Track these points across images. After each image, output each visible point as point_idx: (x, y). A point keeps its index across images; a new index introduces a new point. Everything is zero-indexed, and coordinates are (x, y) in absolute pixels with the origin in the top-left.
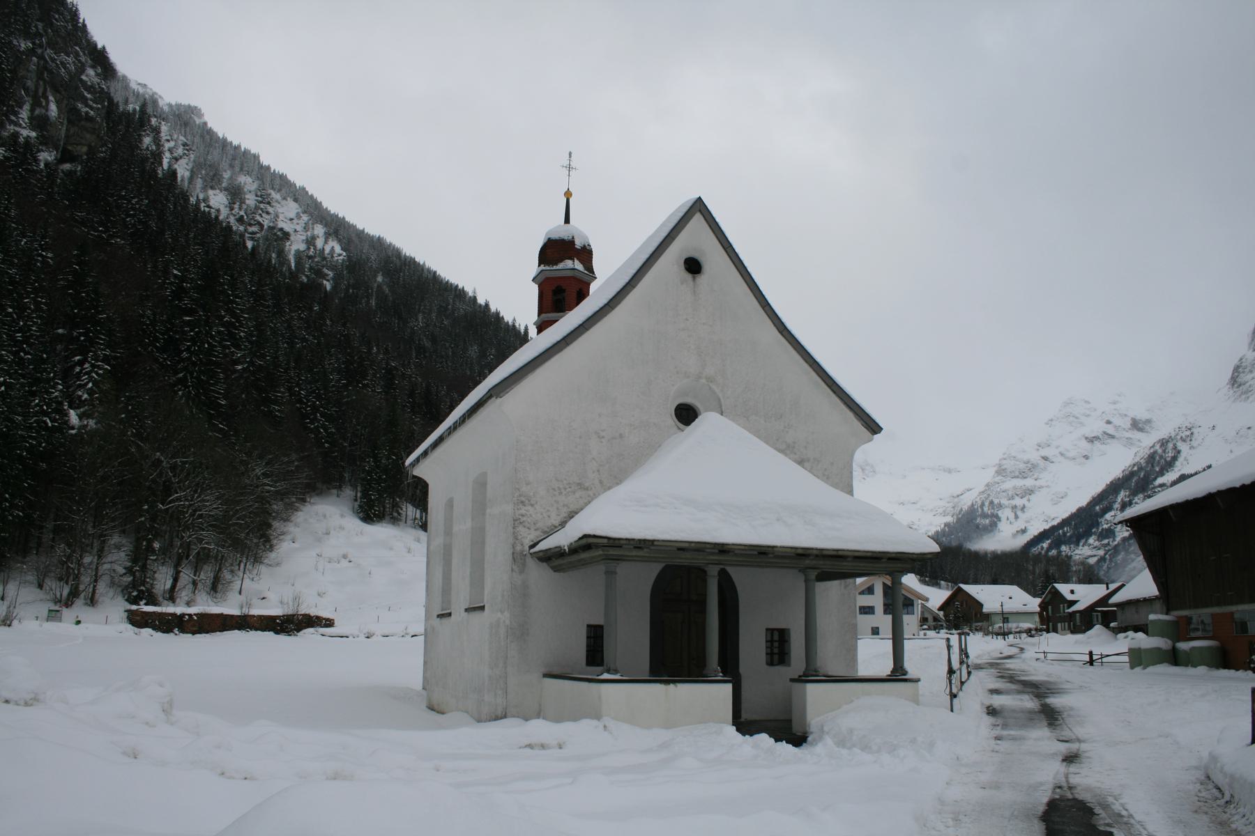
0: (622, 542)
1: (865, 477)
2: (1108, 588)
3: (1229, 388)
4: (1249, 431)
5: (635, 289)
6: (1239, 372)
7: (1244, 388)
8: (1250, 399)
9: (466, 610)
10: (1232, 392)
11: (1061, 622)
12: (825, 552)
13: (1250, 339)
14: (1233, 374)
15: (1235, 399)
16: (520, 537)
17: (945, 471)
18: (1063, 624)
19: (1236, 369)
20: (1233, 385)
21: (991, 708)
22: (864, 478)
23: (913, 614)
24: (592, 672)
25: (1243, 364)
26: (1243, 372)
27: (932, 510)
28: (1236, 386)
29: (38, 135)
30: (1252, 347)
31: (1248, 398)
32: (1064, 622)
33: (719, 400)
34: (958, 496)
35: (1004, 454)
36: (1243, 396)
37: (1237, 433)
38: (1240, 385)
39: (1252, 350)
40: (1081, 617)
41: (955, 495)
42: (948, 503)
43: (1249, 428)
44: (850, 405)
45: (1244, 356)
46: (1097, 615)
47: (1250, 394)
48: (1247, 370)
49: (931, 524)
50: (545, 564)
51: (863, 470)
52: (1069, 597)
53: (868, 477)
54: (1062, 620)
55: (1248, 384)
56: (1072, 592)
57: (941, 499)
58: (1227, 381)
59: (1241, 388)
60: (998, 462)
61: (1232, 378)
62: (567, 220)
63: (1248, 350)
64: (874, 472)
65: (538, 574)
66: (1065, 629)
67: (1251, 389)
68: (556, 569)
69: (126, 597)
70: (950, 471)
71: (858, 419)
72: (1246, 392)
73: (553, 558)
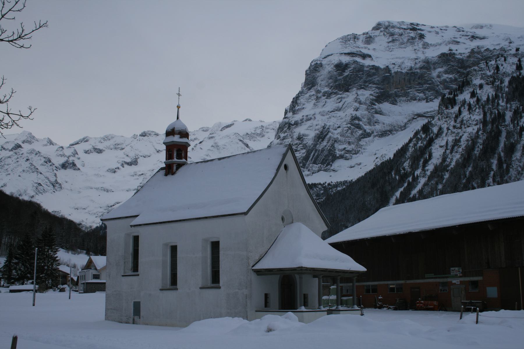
1: (55, 191)
9: (201, 288)
13: (276, 133)
17: (104, 190)
22: (54, 192)
24: (266, 309)
27: (95, 214)
33: (292, 215)
34: (111, 206)
35: (141, 183)
39: (276, 139)
41: (110, 205)
42: (105, 210)
45: (272, 141)
50: (255, 273)
51: (54, 186)
53: (56, 191)
57: (101, 208)
60: (136, 188)
62: (178, 118)
63: (275, 139)
64: (61, 188)
65: (254, 276)
68: (258, 275)
70: (108, 191)
73: (259, 272)
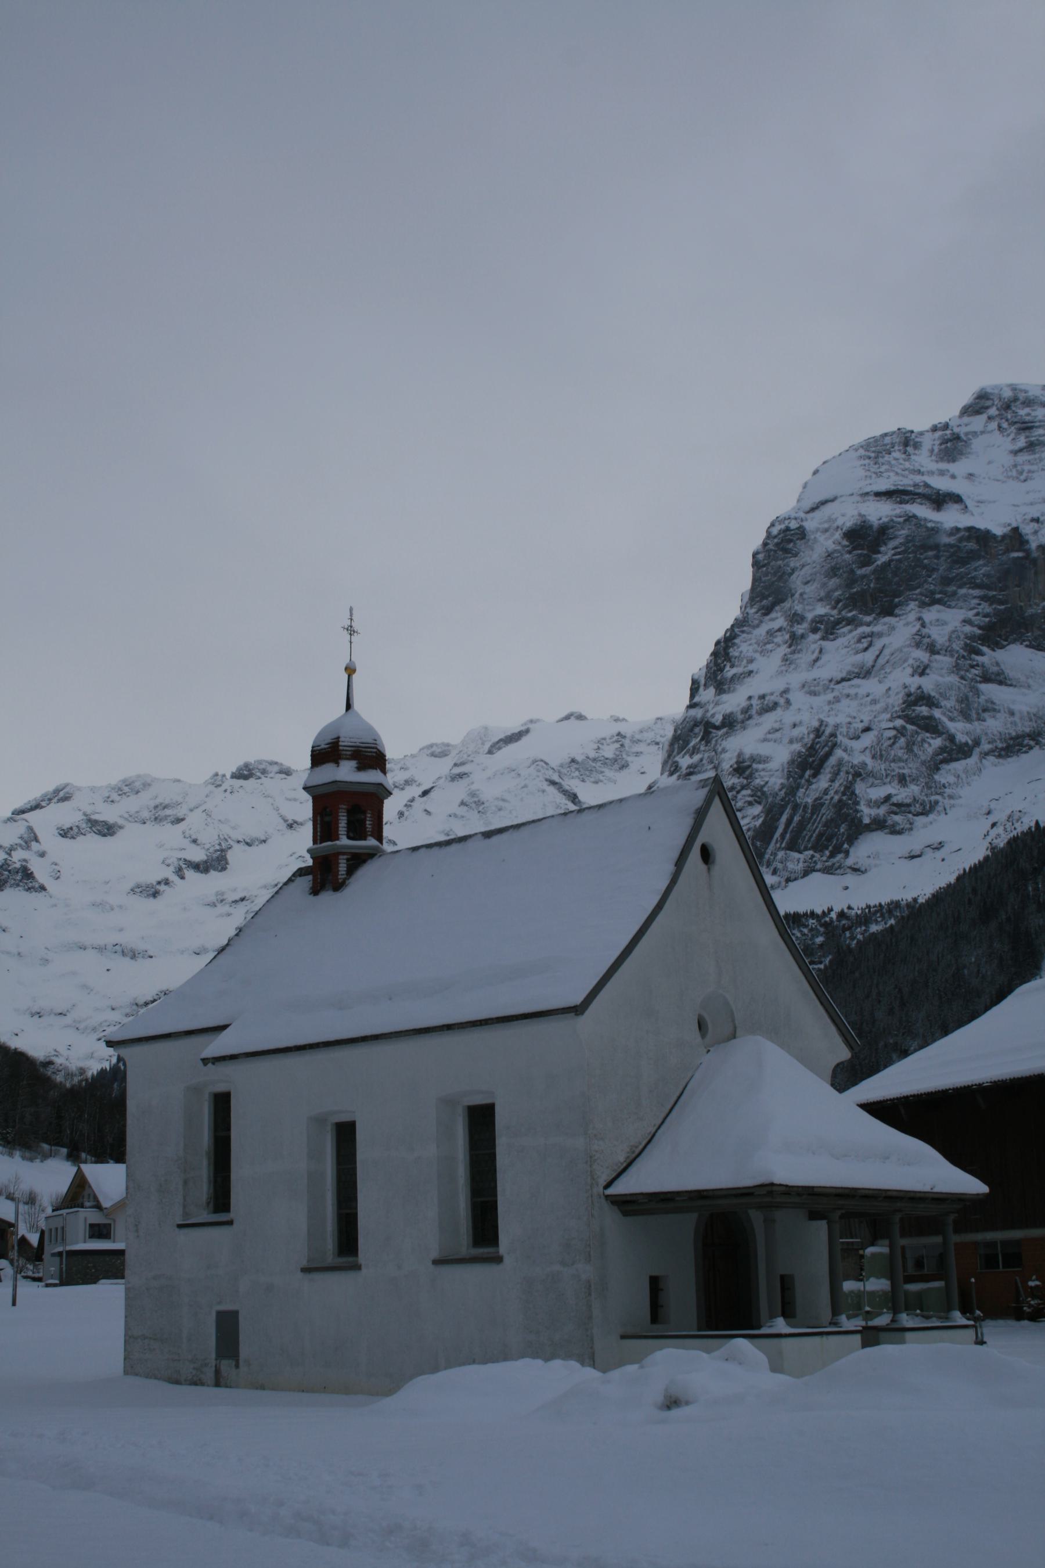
0: (775, 1188)
5: (677, 885)
9: (436, 1262)
12: (889, 1193)
16: (595, 1177)
17: (124, 954)
23: (110, 1238)
27: (94, 1029)
29: (861, 915)
30: (668, 769)
34: (146, 1004)
39: (667, 773)
41: (141, 1001)
42: (127, 1015)
49: (91, 1056)
62: (349, 706)
63: (662, 774)
65: (611, 1218)
68: (625, 1214)
70: (134, 956)
71: (839, 1035)
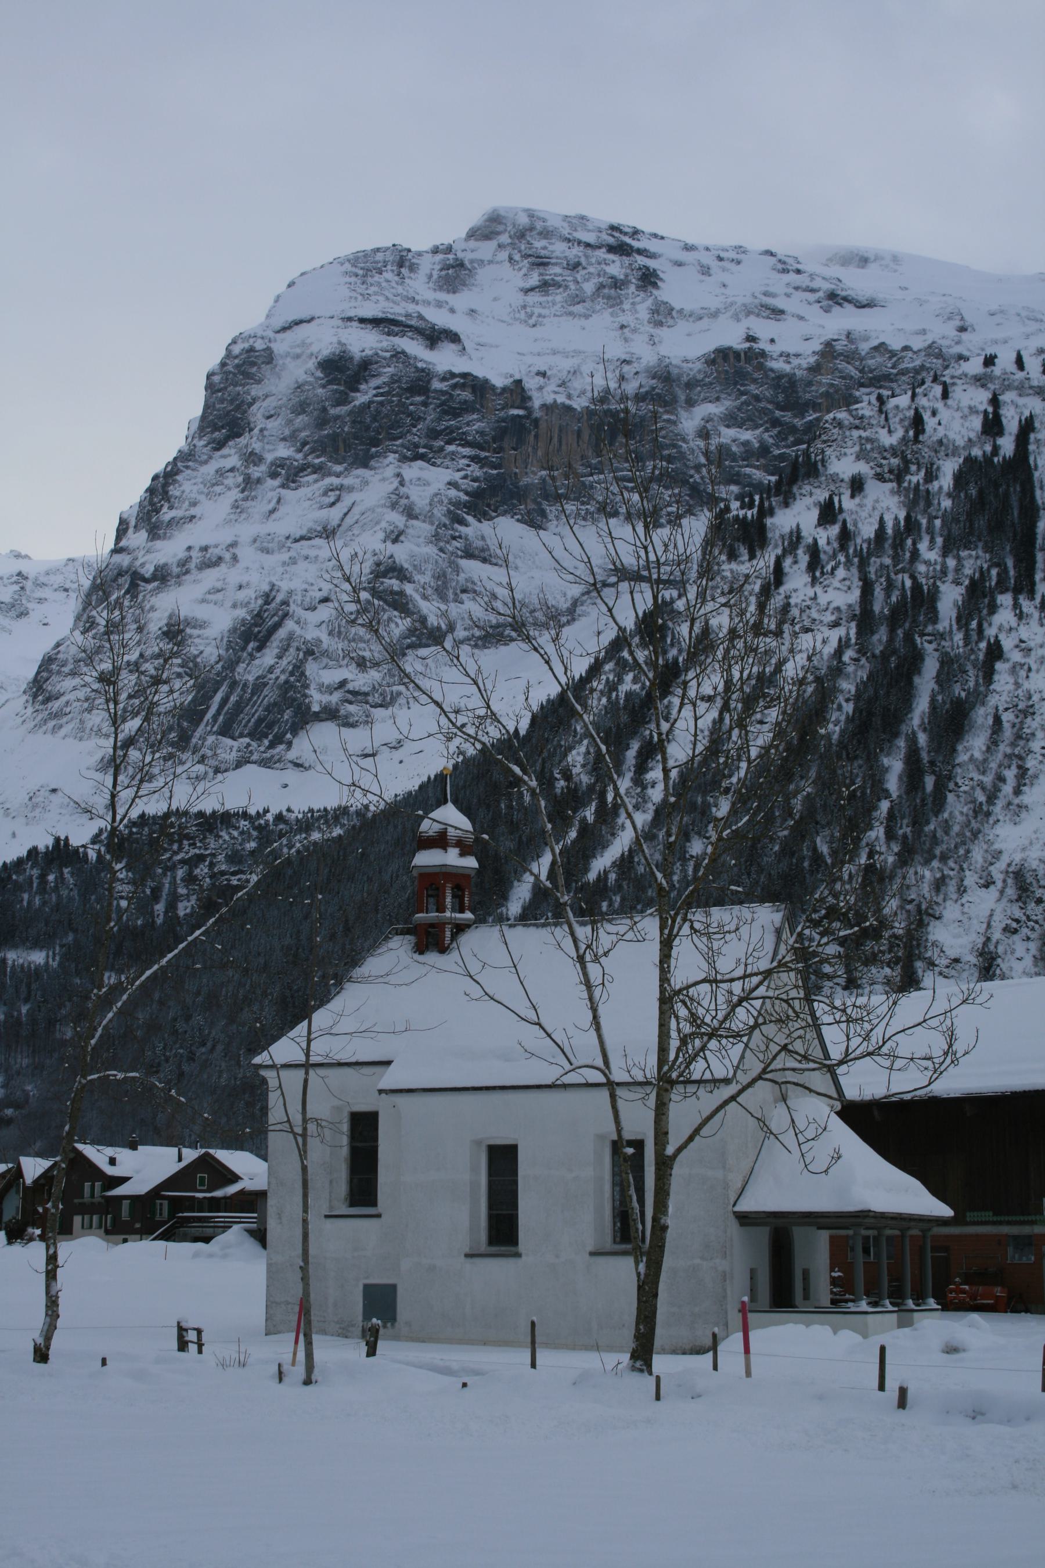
2: (180, 1159)
3: (27, 701)
4: (53, 797)
6: (50, 672)
7: (55, 705)
8: (63, 732)
10: (30, 710)
11: (82, 1214)
14: (38, 673)
15: (35, 726)
18: (87, 1217)
19: (47, 662)
20: (35, 696)
21: (873, 1299)
25: (61, 656)
26: (59, 672)
28: (40, 698)
31: (61, 726)
32: (92, 1214)
36: (51, 724)
37: (31, 799)
38: (48, 700)
40: (132, 1207)
43: (54, 791)
44: (795, 1081)
46: (161, 1204)
47: (65, 719)
48: (66, 670)
52: (110, 1171)
54: (86, 1210)
55: (63, 700)
56: (112, 1161)
58: (24, 686)
59: (50, 705)
61: (35, 680)
66: (91, 1227)
67: (68, 710)
68: (742, 1225)
69: (49, 1268)
72: (56, 716)
